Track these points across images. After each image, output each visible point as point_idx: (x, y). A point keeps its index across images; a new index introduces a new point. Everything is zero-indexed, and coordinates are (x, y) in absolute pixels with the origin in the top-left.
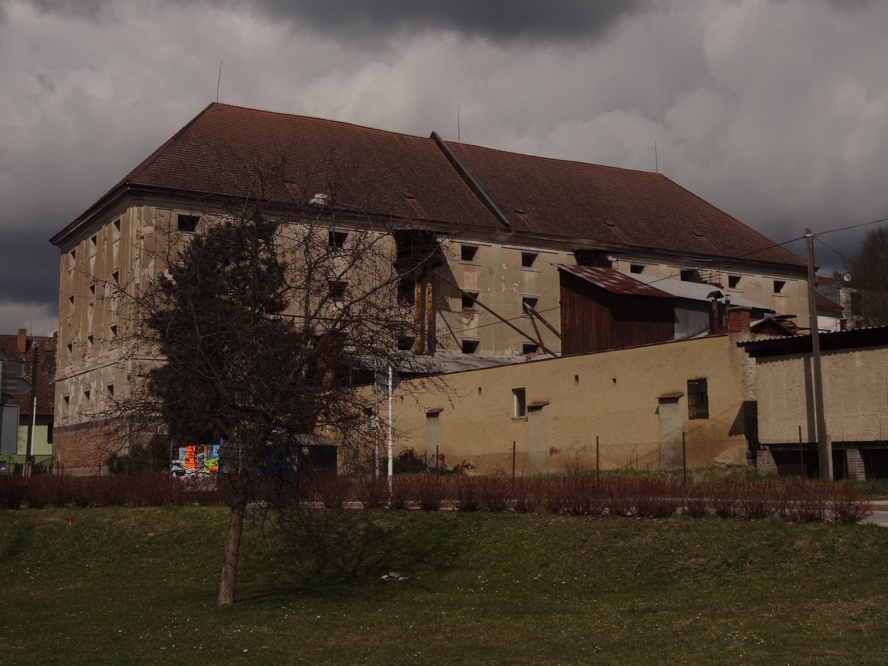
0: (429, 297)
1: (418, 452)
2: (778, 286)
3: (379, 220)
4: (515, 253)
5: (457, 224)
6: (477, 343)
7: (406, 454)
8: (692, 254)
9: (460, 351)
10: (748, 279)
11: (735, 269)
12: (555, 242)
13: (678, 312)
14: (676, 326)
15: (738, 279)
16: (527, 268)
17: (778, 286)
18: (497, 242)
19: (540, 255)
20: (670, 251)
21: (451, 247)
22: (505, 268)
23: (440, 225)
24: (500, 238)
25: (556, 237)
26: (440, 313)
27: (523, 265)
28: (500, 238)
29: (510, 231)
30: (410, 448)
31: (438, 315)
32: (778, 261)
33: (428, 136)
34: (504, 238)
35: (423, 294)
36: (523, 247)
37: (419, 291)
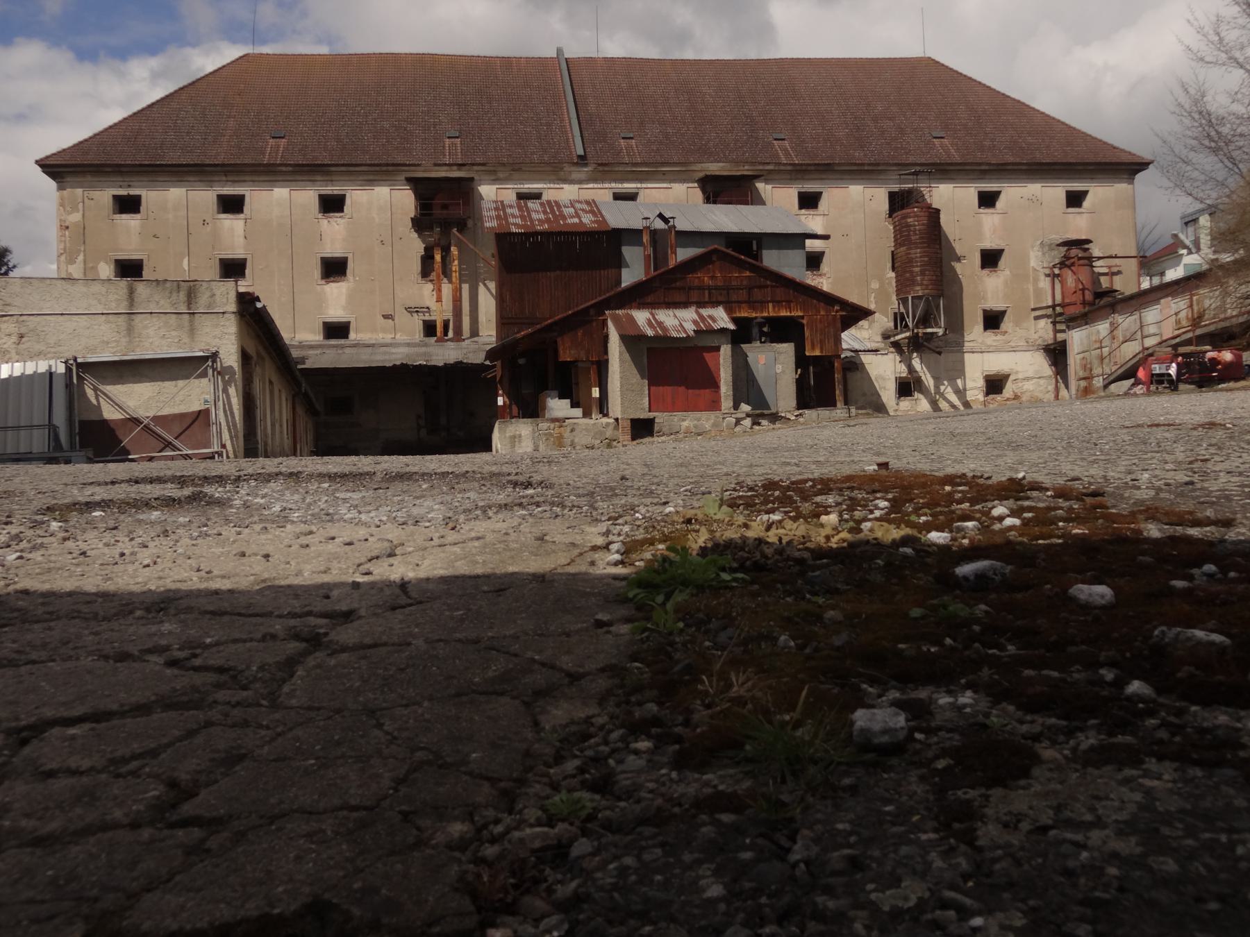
2: (1075, 200)
3: (378, 172)
4: (308, 196)
5: (504, 164)
6: (1003, 313)
10: (1013, 193)
11: (990, 180)
12: (664, 173)
17: (1075, 200)
20: (863, 164)
23: (475, 168)
26: (485, 285)
27: (801, 208)
29: (586, 165)
32: (1099, 160)
34: (583, 176)
36: (613, 185)
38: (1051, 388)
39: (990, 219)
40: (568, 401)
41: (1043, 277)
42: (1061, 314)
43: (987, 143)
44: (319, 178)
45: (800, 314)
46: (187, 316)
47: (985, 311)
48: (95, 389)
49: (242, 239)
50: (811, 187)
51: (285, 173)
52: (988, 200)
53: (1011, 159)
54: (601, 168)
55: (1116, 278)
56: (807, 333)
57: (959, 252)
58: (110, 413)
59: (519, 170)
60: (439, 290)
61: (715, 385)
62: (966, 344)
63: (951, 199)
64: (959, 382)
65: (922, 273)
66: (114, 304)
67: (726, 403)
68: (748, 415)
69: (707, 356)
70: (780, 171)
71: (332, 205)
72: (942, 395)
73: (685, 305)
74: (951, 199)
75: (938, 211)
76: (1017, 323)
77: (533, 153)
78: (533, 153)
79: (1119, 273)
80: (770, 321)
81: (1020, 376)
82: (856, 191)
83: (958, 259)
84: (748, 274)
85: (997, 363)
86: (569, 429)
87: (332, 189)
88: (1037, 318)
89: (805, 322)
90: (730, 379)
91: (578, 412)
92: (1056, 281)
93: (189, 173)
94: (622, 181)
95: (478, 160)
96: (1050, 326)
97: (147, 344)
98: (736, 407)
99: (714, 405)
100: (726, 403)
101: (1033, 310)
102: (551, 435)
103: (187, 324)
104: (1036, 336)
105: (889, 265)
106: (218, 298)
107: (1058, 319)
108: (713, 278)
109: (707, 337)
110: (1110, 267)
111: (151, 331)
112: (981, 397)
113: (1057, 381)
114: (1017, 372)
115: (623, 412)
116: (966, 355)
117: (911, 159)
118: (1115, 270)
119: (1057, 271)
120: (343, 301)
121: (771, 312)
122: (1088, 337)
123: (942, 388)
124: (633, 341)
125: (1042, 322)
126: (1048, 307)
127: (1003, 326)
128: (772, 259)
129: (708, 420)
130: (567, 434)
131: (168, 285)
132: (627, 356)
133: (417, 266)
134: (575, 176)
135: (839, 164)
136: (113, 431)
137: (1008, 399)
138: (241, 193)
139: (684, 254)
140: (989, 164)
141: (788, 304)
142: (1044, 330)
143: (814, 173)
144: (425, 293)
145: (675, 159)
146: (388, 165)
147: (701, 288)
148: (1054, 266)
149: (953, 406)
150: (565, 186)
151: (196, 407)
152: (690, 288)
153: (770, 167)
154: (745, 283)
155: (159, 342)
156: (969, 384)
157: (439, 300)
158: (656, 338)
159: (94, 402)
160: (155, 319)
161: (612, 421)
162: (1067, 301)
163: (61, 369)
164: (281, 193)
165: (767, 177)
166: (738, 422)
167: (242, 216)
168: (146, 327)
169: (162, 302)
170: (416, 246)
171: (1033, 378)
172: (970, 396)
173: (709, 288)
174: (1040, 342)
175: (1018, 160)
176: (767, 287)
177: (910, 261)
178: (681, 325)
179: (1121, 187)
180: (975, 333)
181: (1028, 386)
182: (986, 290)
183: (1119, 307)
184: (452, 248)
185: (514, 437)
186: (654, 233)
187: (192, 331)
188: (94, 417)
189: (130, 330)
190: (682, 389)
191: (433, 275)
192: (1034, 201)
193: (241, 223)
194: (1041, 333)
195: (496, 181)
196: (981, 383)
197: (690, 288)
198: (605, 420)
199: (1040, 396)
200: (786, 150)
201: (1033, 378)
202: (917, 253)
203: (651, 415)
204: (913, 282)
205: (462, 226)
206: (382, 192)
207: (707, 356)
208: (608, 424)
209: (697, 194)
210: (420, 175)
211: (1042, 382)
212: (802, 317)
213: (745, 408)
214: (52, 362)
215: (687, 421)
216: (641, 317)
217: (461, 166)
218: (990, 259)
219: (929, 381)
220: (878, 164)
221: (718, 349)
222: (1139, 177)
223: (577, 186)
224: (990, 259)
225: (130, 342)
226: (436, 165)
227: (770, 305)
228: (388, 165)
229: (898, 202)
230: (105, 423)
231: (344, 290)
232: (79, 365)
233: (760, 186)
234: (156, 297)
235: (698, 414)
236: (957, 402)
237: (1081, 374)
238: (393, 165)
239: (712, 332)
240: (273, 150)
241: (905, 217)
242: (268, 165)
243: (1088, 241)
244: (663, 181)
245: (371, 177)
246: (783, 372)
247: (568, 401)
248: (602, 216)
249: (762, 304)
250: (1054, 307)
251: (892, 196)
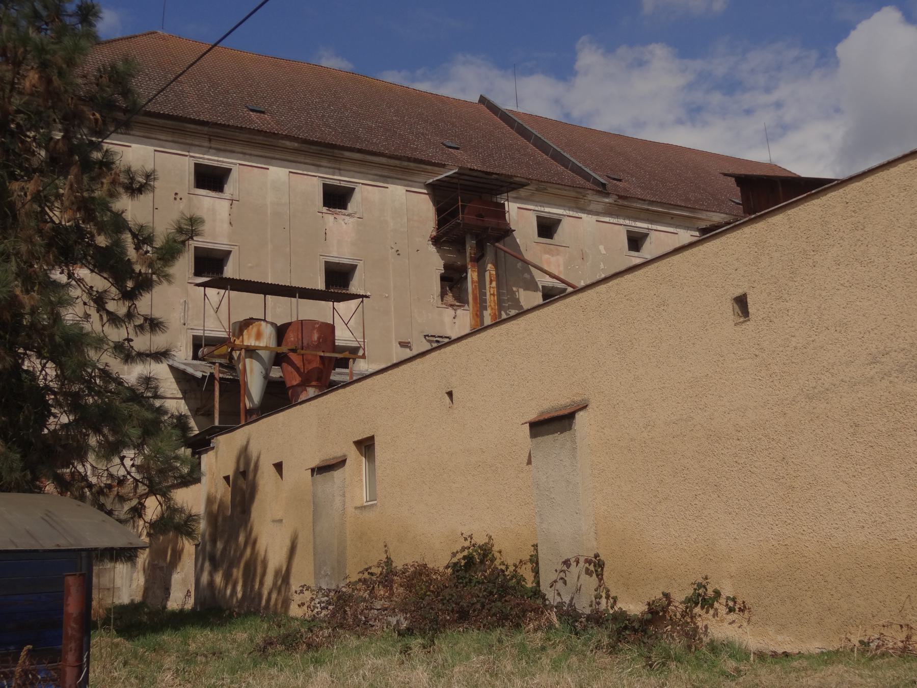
0: (491, 288)
1: (509, 553)
3: (397, 165)
4: (310, 184)
7: (469, 559)
12: (673, 216)
16: (636, 254)
17: (336, 198)
18: (590, 212)
19: (653, 235)
21: (520, 215)
22: (603, 252)
25: (676, 207)
28: (593, 207)
29: (607, 195)
30: (480, 540)
33: (476, 99)
35: (481, 276)
36: (627, 222)
37: (475, 275)
44: (324, 163)
49: (226, 226)
51: (285, 149)
54: (621, 202)
71: (336, 198)
87: (340, 179)
93: (163, 129)
94: (636, 219)
134: (593, 207)
150: (584, 216)
164: (278, 173)
170: (434, 263)
193: (226, 204)
206: (397, 192)
223: (595, 218)
228: (409, 159)
238: (416, 161)
244: (670, 225)
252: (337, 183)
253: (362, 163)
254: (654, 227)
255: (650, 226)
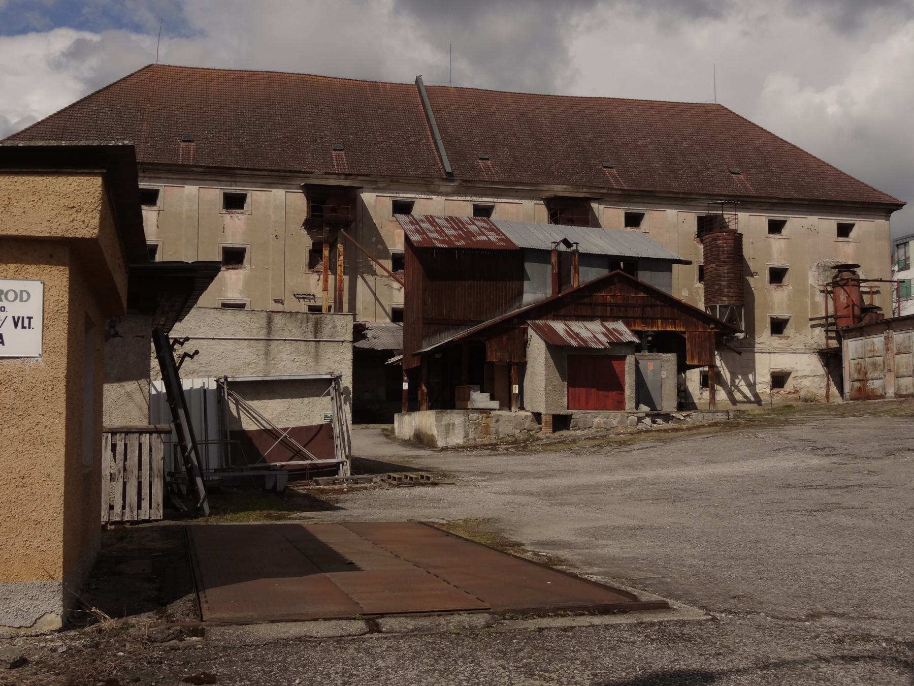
2: (844, 231)
3: (277, 176)
5: (384, 177)
7: (489, 520)
8: (711, 196)
9: (388, 320)
10: (796, 223)
11: (779, 211)
13: (529, 267)
14: (526, 284)
15: (851, 226)
17: (844, 231)
19: (497, 207)
20: (679, 193)
23: (360, 178)
24: (442, 189)
25: (517, 184)
26: (363, 278)
27: (626, 226)
28: (442, 189)
29: (453, 181)
31: (360, 281)
32: (864, 200)
34: (449, 189)
36: (474, 198)
38: (824, 385)
39: (777, 243)
40: (487, 395)
41: (818, 293)
42: (832, 324)
43: (775, 180)
44: (224, 179)
45: (683, 330)
46: (313, 344)
47: (772, 319)
48: (237, 403)
49: (154, 228)
50: (635, 209)
52: (776, 227)
53: (796, 195)
54: (465, 184)
55: (876, 296)
56: (688, 346)
57: (752, 269)
58: (248, 425)
59: (397, 181)
60: (326, 281)
61: (621, 388)
62: (757, 346)
63: (749, 223)
64: (750, 376)
65: (729, 286)
66: (255, 332)
67: (630, 404)
68: (647, 415)
69: (615, 364)
70: (611, 195)
71: (234, 202)
72: (737, 388)
73: (591, 318)
74: (749, 223)
75: (741, 235)
76: (798, 330)
77: (408, 168)
78: (408, 168)
79: (878, 292)
80: (658, 335)
81: (799, 374)
82: (672, 214)
83: (752, 275)
84: (642, 294)
85: (781, 362)
86: (494, 420)
88: (813, 326)
89: (686, 336)
90: (633, 383)
91: (495, 404)
92: (829, 297)
94: (482, 195)
95: (363, 171)
96: (824, 334)
97: (280, 366)
98: (637, 407)
99: (619, 405)
100: (630, 404)
101: (811, 320)
102: (479, 424)
103: (313, 350)
104: (812, 342)
105: (697, 277)
106: (338, 329)
107: (830, 328)
108: (614, 296)
109: (617, 350)
110: (871, 287)
111: (284, 355)
112: (768, 390)
113: (828, 380)
114: (797, 371)
115: (547, 406)
116: (756, 355)
117: (717, 191)
118: (875, 290)
119: (829, 289)
120: (240, 285)
121: (659, 327)
122: (864, 346)
123: (737, 381)
124: (558, 350)
125: (817, 330)
126: (822, 318)
127: (786, 332)
128: (645, 277)
129: (615, 417)
130: (492, 424)
131: (299, 316)
132: (551, 361)
133: (305, 258)
135: (660, 192)
136: (250, 440)
137: (789, 393)
138: (156, 188)
139: (590, 275)
140: (779, 198)
141: (673, 321)
142: (818, 337)
143: (639, 197)
144: (313, 284)
145: (526, 180)
146: (285, 171)
147: (605, 305)
148: (828, 285)
149: (745, 397)
150: (433, 197)
151: (318, 421)
152: (595, 305)
153: (604, 191)
154: (639, 302)
155: (290, 364)
156: (759, 379)
157: (325, 289)
158: (580, 348)
159: (235, 414)
160: (287, 344)
161: (529, 414)
162: (839, 314)
163: (213, 386)
164: (191, 190)
165: (600, 200)
166: (640, 420)
167: (155, 208)
168: (280, 352)
169: (294, 331)
170: (306, 242)
171: (809, 376)
172: (759, 389)
173: (611, 305)
174: (815, 346)
175: (801, 196)
176: (657, 306)
177: (719, 276)
178: (595, 337)
179: (881, 222)
180: (764, 337)
181: (806, 382)
182: (773, 301)
183: (894, 325)
184: (339, 246)
185: (449, 425)
186: (560, 254)
187: (317, 357)
188: (237, 429)
189: (267, 353)
190: (594, 390)
191: (320, 266)
192: (811, 229)
193: (155, 214)
194: (816, 339)
195: (374, 190)
196: (768, 378)
197: (595, 305)
198: (523, 413)
199: (815, 391)
200: (614, 176)
201: (809, 376)
202: (724, 269)
203: (570, 412)
204: (721, 294)
205: (347, 225)
206: (278, 194)
207: (615, 364)
208: (526, 417)
209: (543, 211)
210: (312, 181)
211: (816, 379)
212: (684, 332)
213: (644, 408)
214: (205, 380)
215: (599, 419)
216: (559, 327)
217: (347, 176)
218: (777, 276)
219: (726, 375)
220: (691, 194)
221: (624, 358)
222: (894, 215)
223: (444, 198)
224: (777, 276)
225: (267, 364)
226: (326, 173)
227: (659, 321)
229: (706, 226)
230: (244, 433)
231: (241, 277)
232: (229, 384)
233: (595, 205)
234: (290, 327)
235: (607, 413)
236: (749, 394)
237: (856, 376)
238: (290, 171)
239: (621, 344)
240: (184, 152)
241: (716, 239)
242: (183, 165)
243: (858, 266)
245: (270, 181)
246: (667, 377)
247: (487, 395)
248: (504, 235)
249: (652, 320)
250: (826, 318)
251: (700, 220)
252: (233, 192)
253: (252, 176)
254: (499, 200)
255: (495, 200)
